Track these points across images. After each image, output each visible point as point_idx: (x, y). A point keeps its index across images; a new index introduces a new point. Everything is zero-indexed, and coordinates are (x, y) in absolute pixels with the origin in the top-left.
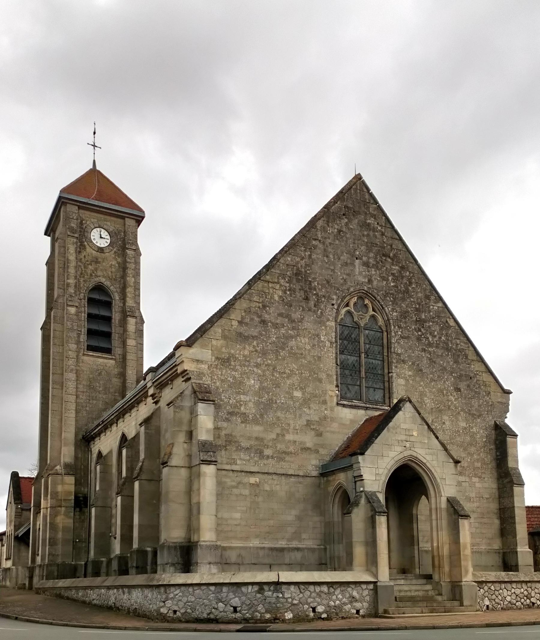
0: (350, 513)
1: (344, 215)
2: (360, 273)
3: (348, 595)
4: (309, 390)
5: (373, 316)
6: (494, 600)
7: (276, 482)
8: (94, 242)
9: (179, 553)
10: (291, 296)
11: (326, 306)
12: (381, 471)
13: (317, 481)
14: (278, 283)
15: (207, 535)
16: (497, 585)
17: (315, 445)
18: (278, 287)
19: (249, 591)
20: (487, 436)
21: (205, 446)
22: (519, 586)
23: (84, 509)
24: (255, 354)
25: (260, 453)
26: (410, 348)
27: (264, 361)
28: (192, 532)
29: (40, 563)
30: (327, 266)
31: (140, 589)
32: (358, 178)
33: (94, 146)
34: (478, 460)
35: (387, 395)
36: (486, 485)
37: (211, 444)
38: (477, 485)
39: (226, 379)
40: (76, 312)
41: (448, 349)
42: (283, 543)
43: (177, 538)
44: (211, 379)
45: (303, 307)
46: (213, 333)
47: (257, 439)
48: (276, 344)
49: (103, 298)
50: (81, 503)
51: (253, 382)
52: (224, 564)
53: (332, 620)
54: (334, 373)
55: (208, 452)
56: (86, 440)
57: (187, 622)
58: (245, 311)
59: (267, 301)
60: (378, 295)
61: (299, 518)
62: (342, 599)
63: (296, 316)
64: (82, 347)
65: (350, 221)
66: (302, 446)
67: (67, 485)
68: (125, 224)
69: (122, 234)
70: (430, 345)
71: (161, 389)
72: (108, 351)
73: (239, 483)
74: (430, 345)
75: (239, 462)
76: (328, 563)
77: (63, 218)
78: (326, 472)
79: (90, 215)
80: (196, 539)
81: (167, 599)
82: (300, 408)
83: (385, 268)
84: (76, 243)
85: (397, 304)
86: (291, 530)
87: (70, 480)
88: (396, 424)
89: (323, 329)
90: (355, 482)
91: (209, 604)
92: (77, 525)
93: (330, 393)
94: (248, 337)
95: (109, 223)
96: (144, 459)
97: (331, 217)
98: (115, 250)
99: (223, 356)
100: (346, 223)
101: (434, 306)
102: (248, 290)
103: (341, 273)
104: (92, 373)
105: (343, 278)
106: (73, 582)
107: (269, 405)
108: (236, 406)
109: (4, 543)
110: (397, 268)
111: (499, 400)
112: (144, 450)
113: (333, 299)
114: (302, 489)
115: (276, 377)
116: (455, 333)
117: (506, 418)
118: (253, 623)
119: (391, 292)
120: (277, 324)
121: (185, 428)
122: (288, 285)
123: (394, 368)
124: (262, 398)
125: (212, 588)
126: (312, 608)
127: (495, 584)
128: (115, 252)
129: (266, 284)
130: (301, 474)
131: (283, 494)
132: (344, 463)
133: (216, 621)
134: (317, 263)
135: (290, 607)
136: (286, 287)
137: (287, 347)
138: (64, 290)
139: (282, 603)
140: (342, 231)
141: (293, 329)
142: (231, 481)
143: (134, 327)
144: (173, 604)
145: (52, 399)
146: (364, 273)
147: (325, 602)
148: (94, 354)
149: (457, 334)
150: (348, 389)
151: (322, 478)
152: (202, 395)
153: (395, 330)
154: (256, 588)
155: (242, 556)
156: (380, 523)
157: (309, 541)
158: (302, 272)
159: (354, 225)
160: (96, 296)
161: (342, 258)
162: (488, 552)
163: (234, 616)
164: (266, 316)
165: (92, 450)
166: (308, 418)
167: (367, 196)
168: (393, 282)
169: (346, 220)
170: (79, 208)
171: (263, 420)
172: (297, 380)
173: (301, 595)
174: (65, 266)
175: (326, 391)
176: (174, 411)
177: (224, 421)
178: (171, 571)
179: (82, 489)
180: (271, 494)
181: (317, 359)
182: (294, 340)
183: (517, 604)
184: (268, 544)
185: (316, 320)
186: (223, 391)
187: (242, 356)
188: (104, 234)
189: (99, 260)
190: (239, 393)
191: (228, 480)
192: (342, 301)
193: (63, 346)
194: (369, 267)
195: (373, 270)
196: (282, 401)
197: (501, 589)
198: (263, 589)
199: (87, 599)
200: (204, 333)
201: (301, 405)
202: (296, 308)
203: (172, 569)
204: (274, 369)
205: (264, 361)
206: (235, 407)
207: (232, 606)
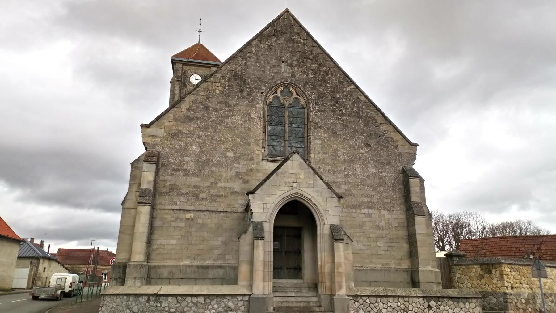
2: (285, 71)
3: (223, 305)
7: (207, 217)
12: (268, 206)
13: (242, 215)
14: (219, 82)
16: (372, 298)
22: (396, 300)
25: (196, 197)
27: (205, 134)
34: (387, 197)
35: (306, 152)
36: (395, 216)
38: (386, 216)
41: (359, 117)
43: (122, 259)
45: (238, 96)
47: (194, 187)
51: (195, 148)
58: (193, 102)
61: (225, 243)
65: (278, 38)
70: (343, 115)
73: (177, 218)
74: (343, 115)
75: (178, 203)
82: (231, 164)
85: (315, 89)
86: (217, 252)
94: (193, 118)
107: (206, 163)
110: (316, 65)
122: (227, 83)
127: (370, 298)
130: (229, 210)
131: (213, 226)
134: (251, 68)
141: (230, 111)
149: (367, 106)
154: (146, 298)
156: (258, 246)
162: (397, 270)
166: (237, 171)
167: (293, 22)
169: (275, 39)
170: (183, 65)
173: (178, 305)
180: (203, 226)
184: (196, 263)
191: (168, 216)
197: (376, 302)
203: (114, 282)
204: (212, 138)
205: (205, 134)
206: (179, 166)
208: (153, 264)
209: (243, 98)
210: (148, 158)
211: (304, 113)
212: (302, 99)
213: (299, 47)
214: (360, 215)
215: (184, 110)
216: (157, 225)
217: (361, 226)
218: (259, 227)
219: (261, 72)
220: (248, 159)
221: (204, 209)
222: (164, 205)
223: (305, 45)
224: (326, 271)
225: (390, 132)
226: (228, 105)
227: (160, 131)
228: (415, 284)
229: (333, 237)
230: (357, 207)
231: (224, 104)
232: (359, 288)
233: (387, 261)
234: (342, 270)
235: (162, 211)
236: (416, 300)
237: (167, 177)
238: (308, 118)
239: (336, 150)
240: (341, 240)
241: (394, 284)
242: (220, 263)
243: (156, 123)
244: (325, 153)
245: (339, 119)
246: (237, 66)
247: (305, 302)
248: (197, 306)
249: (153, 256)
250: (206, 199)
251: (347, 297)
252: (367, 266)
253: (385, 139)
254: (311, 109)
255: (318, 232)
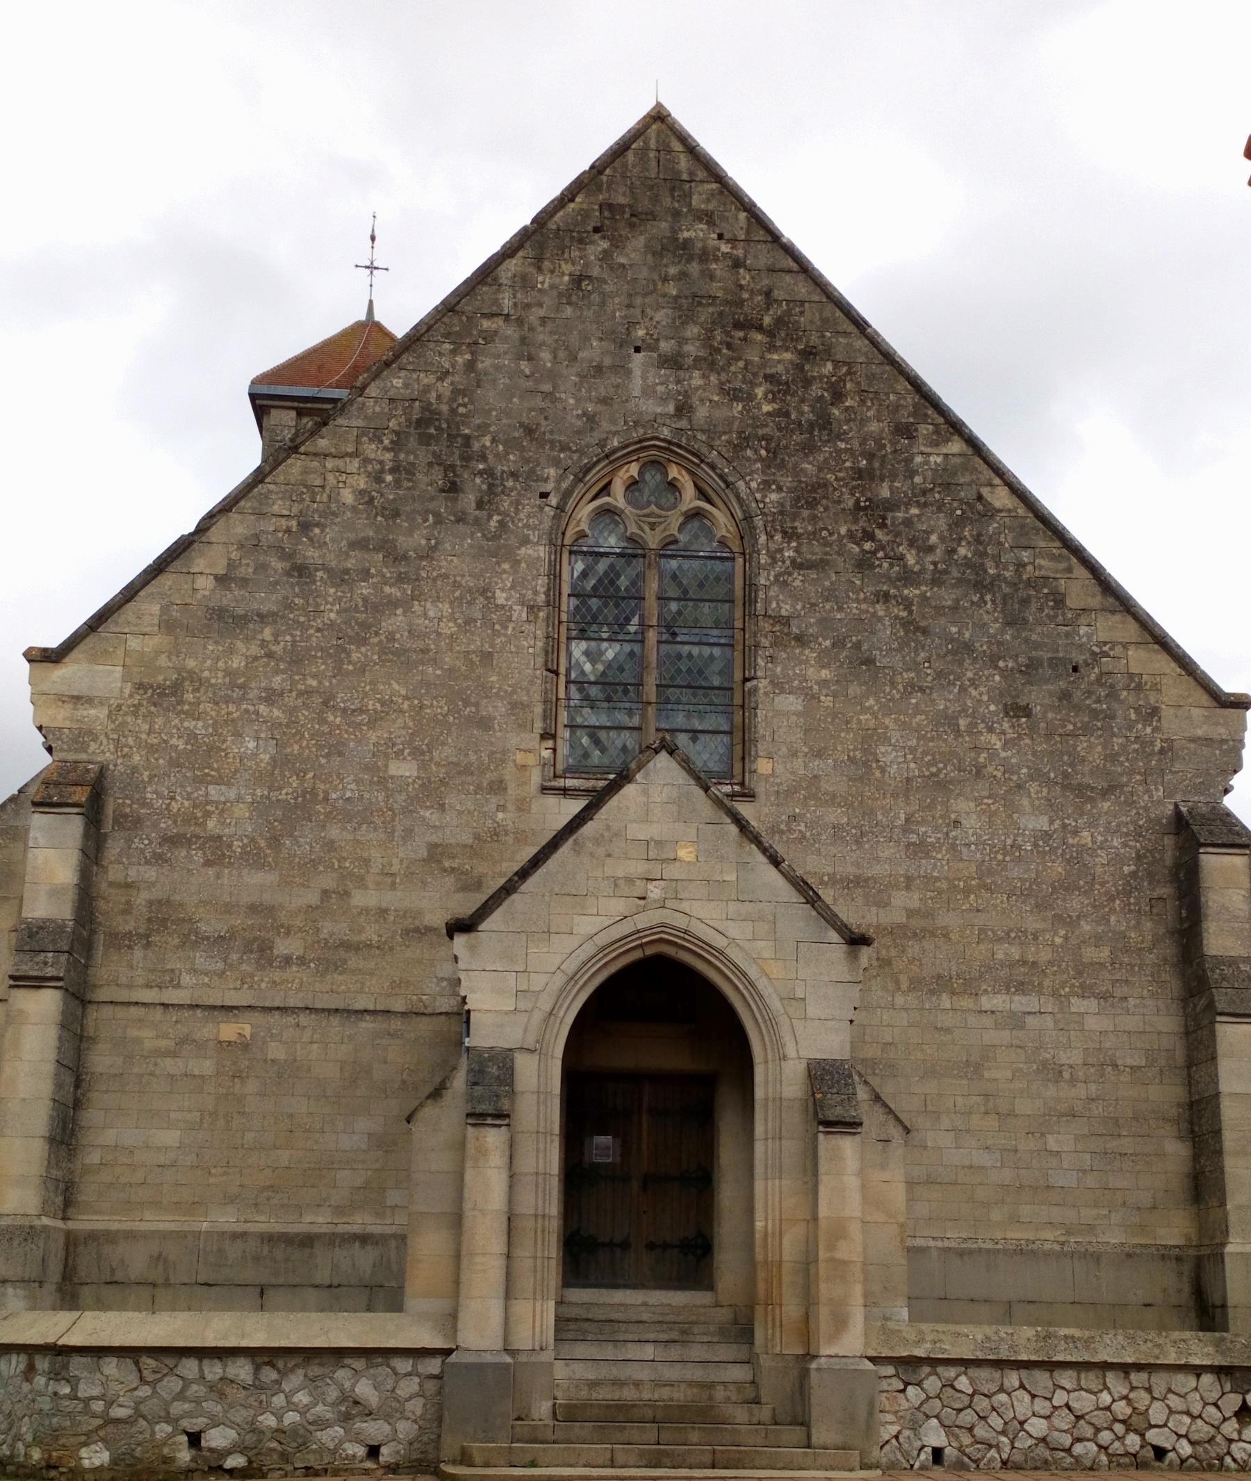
1: (597, 230)
2: (648, 391)
3: (333, 1394)
6: (970, 1430)
11: (518, 503)
12: (538, 981)
14: (356, 454)
16: (983, 1373)
18: (354, 465)
20: (1139, 857)
22: (1090, 1380)
25: (262, 951)
26: (829, 594)
27: (294, 683)
30: (530, 384)
34: (1098, 940)
35: (738, 748)
36: (1132, 1023)
38: (1092, 1023)
41: (982, 585)
42: (321, 1220)
44: (116, 748)
45: (437, 515)
47: (253, 909)
48: (340, 631)
51: (252, 745)
58: (241, 546)
60: (712, 448)
62: (308, 1408)
63: (412, 540)
65: (617, 243)
66: (408, 923)
70: (908, 578)
73: (183, 1041)
74: (908, 578)
75: (186, 979)
82: (407, 811)
83: (741, 364)
85: (782, 465)
88: (608, 828)
89: (504, 571)
93: (520, 758)
97: (551, 243)
99: (160, 678)
100: (605, 251)
101: (929, 454)
103: (578, 400)
105: (584, 414)
110: (788, 356)
111: (1199, 732)
115: (330, 724)
116: (1011, 529)
117: (1226, 791)
119: (760, 432)
120: (347, 571)
122: (389, 456)
123: (761, 662)
124: (281, 789)
126: (188, 1434)
127: (973, 1372)
129: (315, 464)
130: (399, 1006)
134: (494, 381)
136: (381, 463)
137: (377, 634)
140: (589, 277)
141: (401, 579)
146: (660, 389)
147: (240, 1415)
149: (1022, 530)
153: (773, 547)
155: (166, 1261)
156: (482, 1152)
158: (439, 413)
162: (1129, 1255)
166: (435, 839)
167: (683, 162)
172: (405, 727)
173: (145, 1391)
175: (505, 752)
177: (147, 862)
182: (399, 611)
183: (1078, 1449)
184: (264, 1223)
186: (151, 777)
187: (220, 674)
190: (203, 781)
191: (146, 1033)
194: (680, 368)
196: (348, 794)
197: (1002, 1389)
204: (325, 703)
205: (294, 683)
206: (187, 822)
208: (88, 1226)
209: (458, 520)
210: (52, 790)
211: (730, 578)
212: (720, 516)
213: (712, 277)
214: (972, 1020)
215: (205, 584)
216: (99, 1069)
217: (974, 1068)
218: (494, 1070)
219: (538, 402)
220: (479, 788)
221: (292, 1003)
222: (130, 987)
223: (737, 264)
224: (786, 1257)
225: (1125, 646)
226: (395, 556)
227: (103, 677)
228: (1207, 1312)
229: (816, 1113)
230: (957, 984)
231: (376, 550)
232: (925, 1327)
233: (1088, 1214)
234: (851, 1250)
235: (121, 1012)
236: (1185, 1382)
237: (133, 869)
238: (749, 600)
239: (870, 738)
240: (850, 1126)
241: (1111, 1315)
242: (361, 1222)
243: (91, 640)
244: (819, 754)
245: (886, 596)
246: (430, 379)
247: (691, 1384)
248: (222, 1395)
249: (87, 1193)
250: (302, 961)
251: (869, 1365)
252: (998, 1235)
253: (1098, 680)
254: (764, 559)
255: (759, 1093)
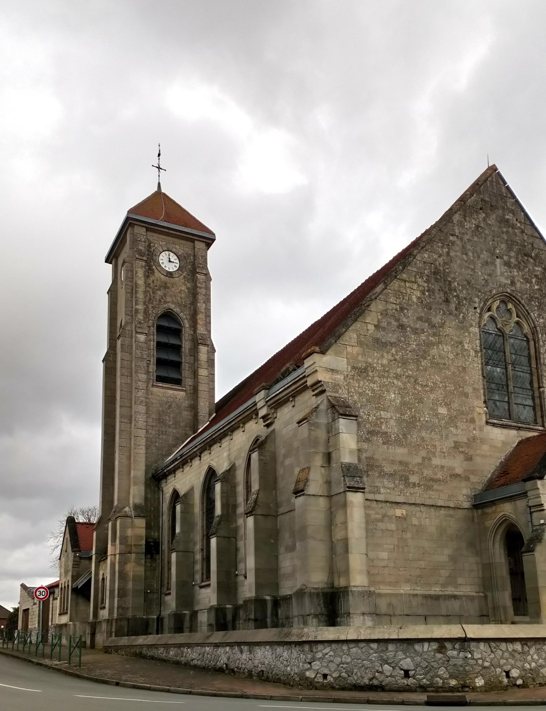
0: (533, 551)
1: (481, 209)
2: (502, 274)
4: (455, 406)
5: (518, 323)
7: (424, 515)
8: (163, 266)
9: (321, 602)
10: (430, 298)
14: (415, 282)
15: (358, 580)
17: (465, 471)
18: (415, 286)
19: (426, 649)
21: (349, 471)
23: (155, 556)
24: (394, 364)
25: (405, 480)
27: (404, 372)
28: (336, 575)
29: (107, 618)
31: (268, 647)
32: (493, 169)
33: (159, 168)
37: (356, 467)
39: (365, 392)
40: (144, 340)
42: (437, 589)
45: (443, 311)
46: (348, 339)
47: (401, 463)
48: (417, 353)
49: (173, 325)
50: (152, 548)
51: (393, 396)
52: (376, 615)
53: (528, 687)
54: (481, 386)
55: (354, 477)
56: (156, 478)
57: (343, 689)
58: (382, 314)
59: (405, 303)
60: (522, 299)
61: (453, 559)
62: (538, 660)
63: (437, 319)
64: (152, 378)
65: (487, 216)
67: (138, 528)
68: (194, 247)
69: (192, 257)
71: (276, 409)
72: (178, 382)
75: (382, 490)
76: (490, 614)
77: (130, 241)
78: (481, 504)
79: (158, 237)
80: (342, 583)
81: (314, 659)
83: (527, 269)
84: (145, 267)
86: (444, 573)
87: (141, 523)
89: (466, 336)
90: (531, 513)
91: (370, 666)
92: (148, 573)
94: (385, 343)
95: (177, 247)
96: (259, 490)
97: (468, 211)
98: (184, 274)
99: (360, 365)
100: (484, 218)
102: (384, 289)
103: (482, 273)
104: (161, 405)
105: (484, 279)
106: (159, 639)
107: (410, 425)
108: (376, 425)
109: (55, 596)
110: (540, 269)
112: (258, 480)
113: (475, 302)
114: (454, 524)
115: (418, 390)
118: (432, 691)
119: (536, 296)
120: (417, 329)
121: (322, 449)
122: (426, 285)
124: (404, 415)
125: (374, 646)
128: (184, 277)
130: (452, 505)
131: (433, 530)
132: (515, 489)
133: (381, 688)
135: (481, 670)
136: (424, 287)
138: (132, 316)
139: (472, 666)
141: (434, 335)
142: (375, 514)
143: (206, 356)
144: (322, 666)
145: (120, 435)
146: (506, 274)
147: (519, 664)
148: (164, 385)
150: (496, 406)
151: (475, 511)
152: (340, 409)
154: (435, 646)
157: (467, 588)
158: (440, 270)
159: (492, 220)
160: (165, 323)
161: (482, 256)
163: (405, 681)
164: (405, 320)
165: (164, 489)
167: (504, 190)
168: (538, 285)
169: (484, 215)
170: (148, 229)
171: (406, 441)
173: (492, 656)
174: (132, 291)
176: (309, 429)
177: (364, 441)
178: (314, 623)
179: (152, 534)
180: (419, 530)
181: (461, 369)
182: (435, 347)
184: (420, 591)
185: (458, 326)
186: (362, 406)
187: (380, 366)
188: (173, 258)
189: (168, 285)
190: (378, 409)
192: (485, 304)
193: (131, 376)
195: (515, 270)
196: (426, 419)
198: (445, 647)
199: (182, 659)
200: (339, 338)
201: (447, 423)
202: (436, 312)
204: (415, 381)
205: (404, 372)
206: (375, 425)
207: (402, 669)
